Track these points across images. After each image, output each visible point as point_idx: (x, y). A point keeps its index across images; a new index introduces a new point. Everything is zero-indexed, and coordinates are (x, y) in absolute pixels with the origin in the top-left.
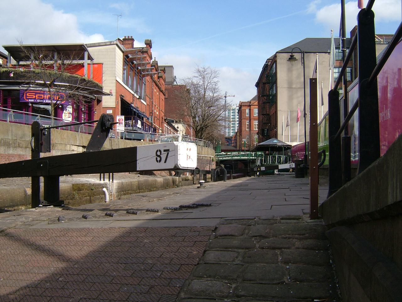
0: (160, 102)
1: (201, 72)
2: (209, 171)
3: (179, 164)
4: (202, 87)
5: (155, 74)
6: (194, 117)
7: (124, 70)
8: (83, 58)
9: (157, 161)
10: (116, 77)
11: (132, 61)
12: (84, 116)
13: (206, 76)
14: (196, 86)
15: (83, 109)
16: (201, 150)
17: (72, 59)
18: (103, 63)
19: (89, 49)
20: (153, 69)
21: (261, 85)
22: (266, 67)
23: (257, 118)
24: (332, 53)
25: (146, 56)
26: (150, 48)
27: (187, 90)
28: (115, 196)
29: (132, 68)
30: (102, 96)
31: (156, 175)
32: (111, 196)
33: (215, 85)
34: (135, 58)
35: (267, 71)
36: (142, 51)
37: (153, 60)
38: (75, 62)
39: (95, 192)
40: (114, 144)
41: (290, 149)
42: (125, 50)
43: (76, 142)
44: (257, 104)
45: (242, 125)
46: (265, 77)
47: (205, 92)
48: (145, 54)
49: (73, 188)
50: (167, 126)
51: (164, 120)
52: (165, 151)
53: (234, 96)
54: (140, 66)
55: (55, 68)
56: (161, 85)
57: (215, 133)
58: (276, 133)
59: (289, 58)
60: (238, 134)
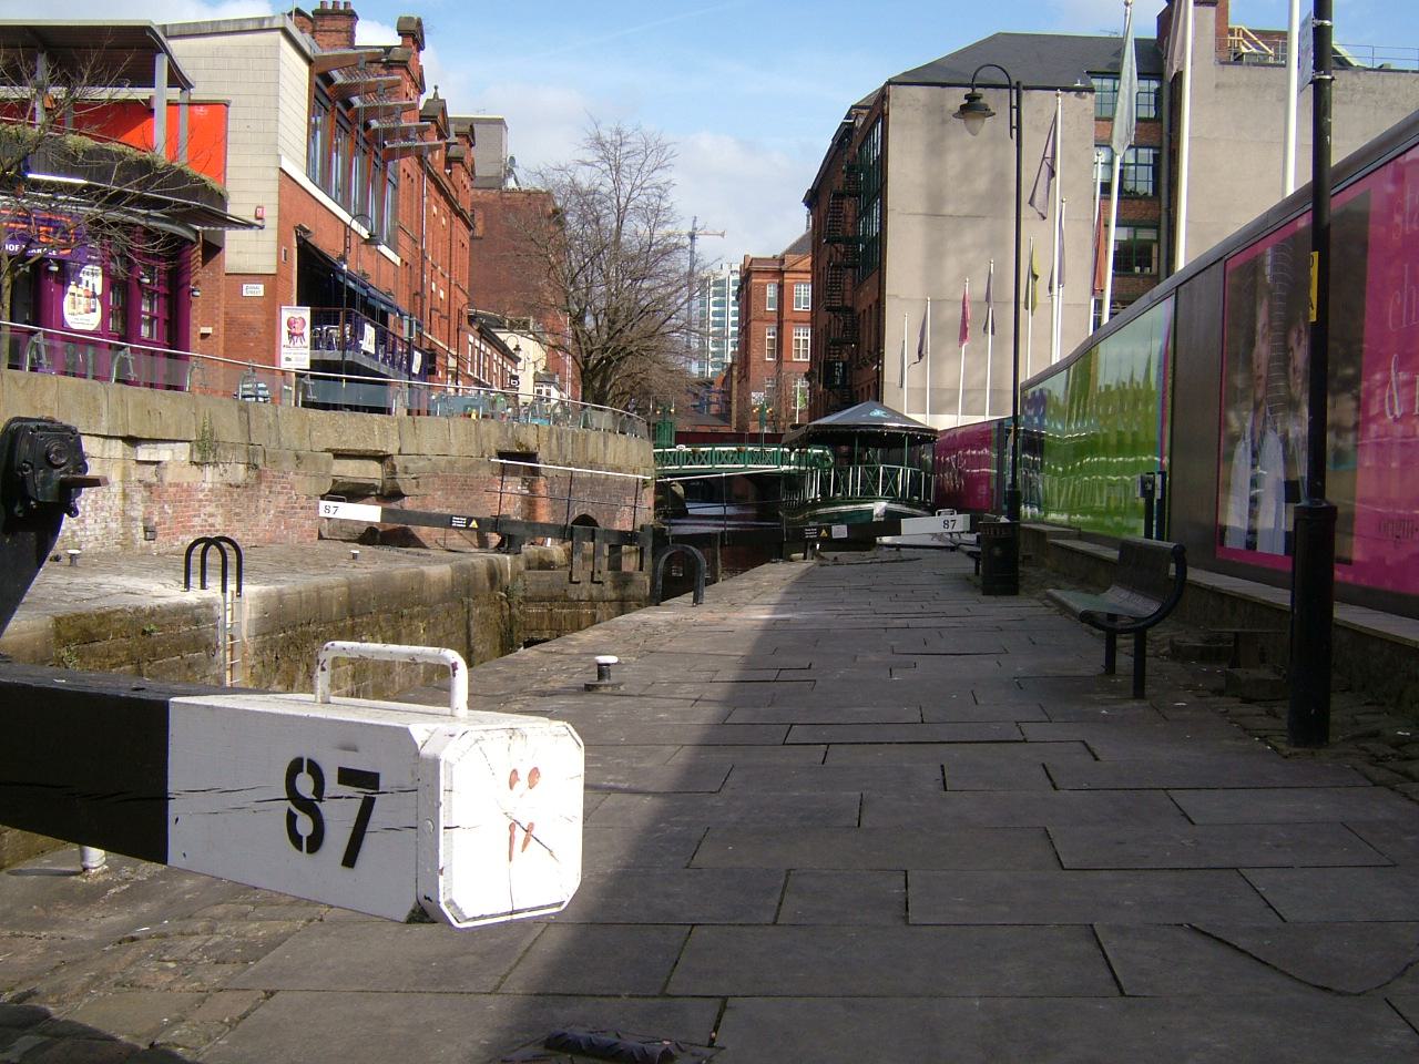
0: (453, 253)
1: (608, 146)
2: (631, 532)
3: (451, 903)
4: (609, 204)
5: (433, 148)
6: (578, 319)
7: (312, 129)
8: (149, 82)
9: (295, 839)
10: (279, 155)
11: (344, 95)
12: (151, 305)
13: (628, 162)
14: (587, 200)
15: (147, 281)
16: (601, 445)
17: (85, 81)
18: (228, 101)
19: (174, 45)
20: (427, 129)
21: (826, 201)
22: (845, 136)
23: (808, 317)
24: (1127, 92)
25: (399, 77)
26: (418, 51)
27: (556, 212)
28: (251, 651)
29: (343, 122)
30: (223, 233)
31: (427, 544)
32: (232, 650)
33: (660, 197)
34: (357, 85)
35: (851, 150)
36: (385, 59)
37: (428, 94)
38: (124, 93)
39: (160, 642)
40: (258, 427)
41: (931, 442)
42: (319, 52)
43: (98, 422)
44: (809, 268)
45: (752, 342)
46: (844, 172)
47: (620, 221)
48: (399, 71)
49: (58, 635)
50: (477, 343)
51: (465, 321)
52: (348, 776)
53: (722, 235)
54: (377, 118)
55: (40, 118)
56: (457, 191)
57: (656, 378)
58: (878, 377)
59: (962, 107)
60: (735, 373)
